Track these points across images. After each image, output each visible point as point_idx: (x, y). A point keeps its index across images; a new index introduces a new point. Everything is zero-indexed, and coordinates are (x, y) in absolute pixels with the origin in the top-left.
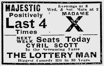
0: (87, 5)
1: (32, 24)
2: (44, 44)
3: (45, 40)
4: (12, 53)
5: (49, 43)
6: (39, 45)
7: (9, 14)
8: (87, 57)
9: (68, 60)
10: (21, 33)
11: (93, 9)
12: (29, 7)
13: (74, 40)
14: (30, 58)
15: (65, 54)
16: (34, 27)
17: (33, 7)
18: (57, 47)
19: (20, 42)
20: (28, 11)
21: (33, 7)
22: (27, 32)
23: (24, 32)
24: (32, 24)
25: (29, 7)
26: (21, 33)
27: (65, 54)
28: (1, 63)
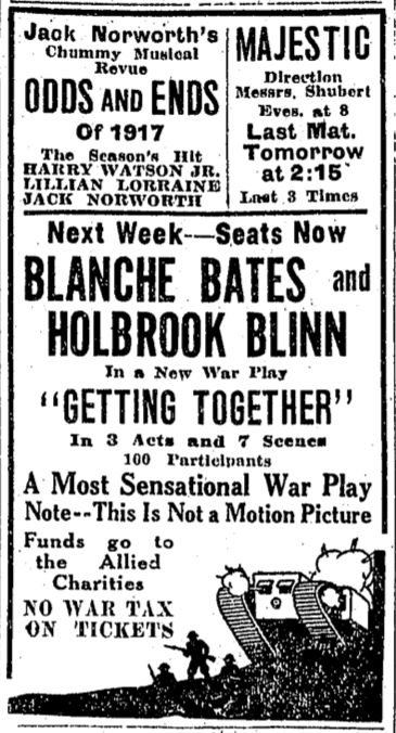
0: (341, 113)
1: (104, 488)
2: (47, 402)
3: (306, 577)
5: (79, 140)
7: (161, 565)
8: (281, 234)
9: (340, 76)
11: (274, 194)
12: (322, 40)
14: (203, 300)
15: (77, 167)
16: (108, 493)
17: (339, 37)
18: (127, 474)
20: (174, 312)
21: (339, 37)
22: (288, 153)
23: (281, 153)
24: (104, 488)
25: (322, 40)
27: (77, 167)
28: (199, 297)
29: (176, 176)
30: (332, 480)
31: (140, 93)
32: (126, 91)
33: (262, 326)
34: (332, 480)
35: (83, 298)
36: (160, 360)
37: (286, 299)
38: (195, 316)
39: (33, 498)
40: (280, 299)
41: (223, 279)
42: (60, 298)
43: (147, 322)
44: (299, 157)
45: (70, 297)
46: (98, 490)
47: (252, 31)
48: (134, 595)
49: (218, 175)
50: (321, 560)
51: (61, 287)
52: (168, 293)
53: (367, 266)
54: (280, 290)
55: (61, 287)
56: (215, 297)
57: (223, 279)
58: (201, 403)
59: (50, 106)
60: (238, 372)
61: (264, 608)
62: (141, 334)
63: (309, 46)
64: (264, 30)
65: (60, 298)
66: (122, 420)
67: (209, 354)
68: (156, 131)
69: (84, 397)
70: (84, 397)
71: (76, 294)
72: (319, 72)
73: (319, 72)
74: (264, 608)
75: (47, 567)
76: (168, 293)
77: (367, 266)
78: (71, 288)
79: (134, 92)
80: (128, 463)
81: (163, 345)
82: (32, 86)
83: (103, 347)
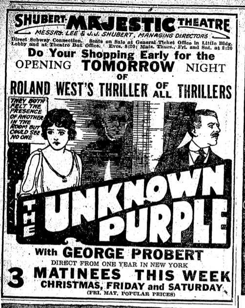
2: (129, 85)
6: (59, 283)
13: (104, 264)
19: (41, 254)
30: (28, 62)
31: (49, 83)
32: (42, 82)
33: (196, 90)
34: (28, 62)
37: (207, 20)
40: (69, 94)
42: (28, 93)
44: (98, 57)
45: (31, 93)
46: (75, 92)
50: (169, 236)
51: (28, 90)
52: (137, 94)
54: (69, 91)
55: (28, 90)
58: (102, 88)
60: (190, 55)
62: (114, 90)
63: (72, 91)
65: (28, 93)
71: (32, 93)
72: (121, 41)
73: (121, 41)
75: (203, 59)
76: (137, 94)
78: (31, 91)
79: (46, 83)
83: (132, 94)
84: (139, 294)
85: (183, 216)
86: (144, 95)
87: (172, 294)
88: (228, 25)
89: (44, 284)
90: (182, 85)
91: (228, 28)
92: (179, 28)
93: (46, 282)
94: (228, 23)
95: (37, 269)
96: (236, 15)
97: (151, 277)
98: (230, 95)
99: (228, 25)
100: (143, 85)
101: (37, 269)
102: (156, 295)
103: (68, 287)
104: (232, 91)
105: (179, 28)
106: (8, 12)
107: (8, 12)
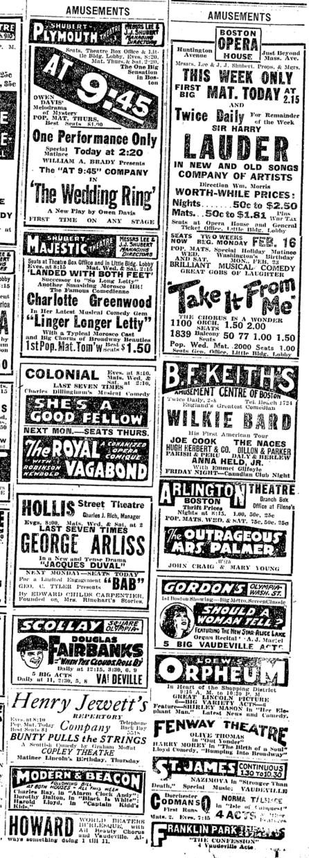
4: (266, 727)
10: (37, 201)
26: (37, 201)
29: (253, 37)
35: (98, 553)
36: (74, 205)
38: (262, 89)
39: (98, 740)
41: (120, 583)
43: (107, 539)
47: (37, 818)
48: (98, 591)
49: (232, 111)
53: (150, 297)
56: (118, 588)
57: (120, 583)
59: (69, 832)
61: (139, 420)
64: (34, 834)
66: (245, 98)
67: (16, 817)
68: (177, 294)
69: (73, 539)
70: (73, 539)
74: (139, 420)
77: (150, 297)
80: (172, 336)
81: (27, 822)
82: (24, 831)
84: (249, 215)
85: (143, 472)
86: (26, 513)
87: (74, 600)
88: (284, 736)
89: (182, 174)
90: (266, 727)
91: (283, 739)
92: (135, 351)
93: (33, 371)
94: (284, 732)
95: (223, 797)
96: (22, 357)
97: (96, 551)
98: (143, 550)
99: (273, 833)
100: (278, 139)
101: (223, 797)
102: (259, 196)
103: (68, 513)
104: (146, 544)
105: (135, 351)
106: (148, 606)
107: (148, 606)
